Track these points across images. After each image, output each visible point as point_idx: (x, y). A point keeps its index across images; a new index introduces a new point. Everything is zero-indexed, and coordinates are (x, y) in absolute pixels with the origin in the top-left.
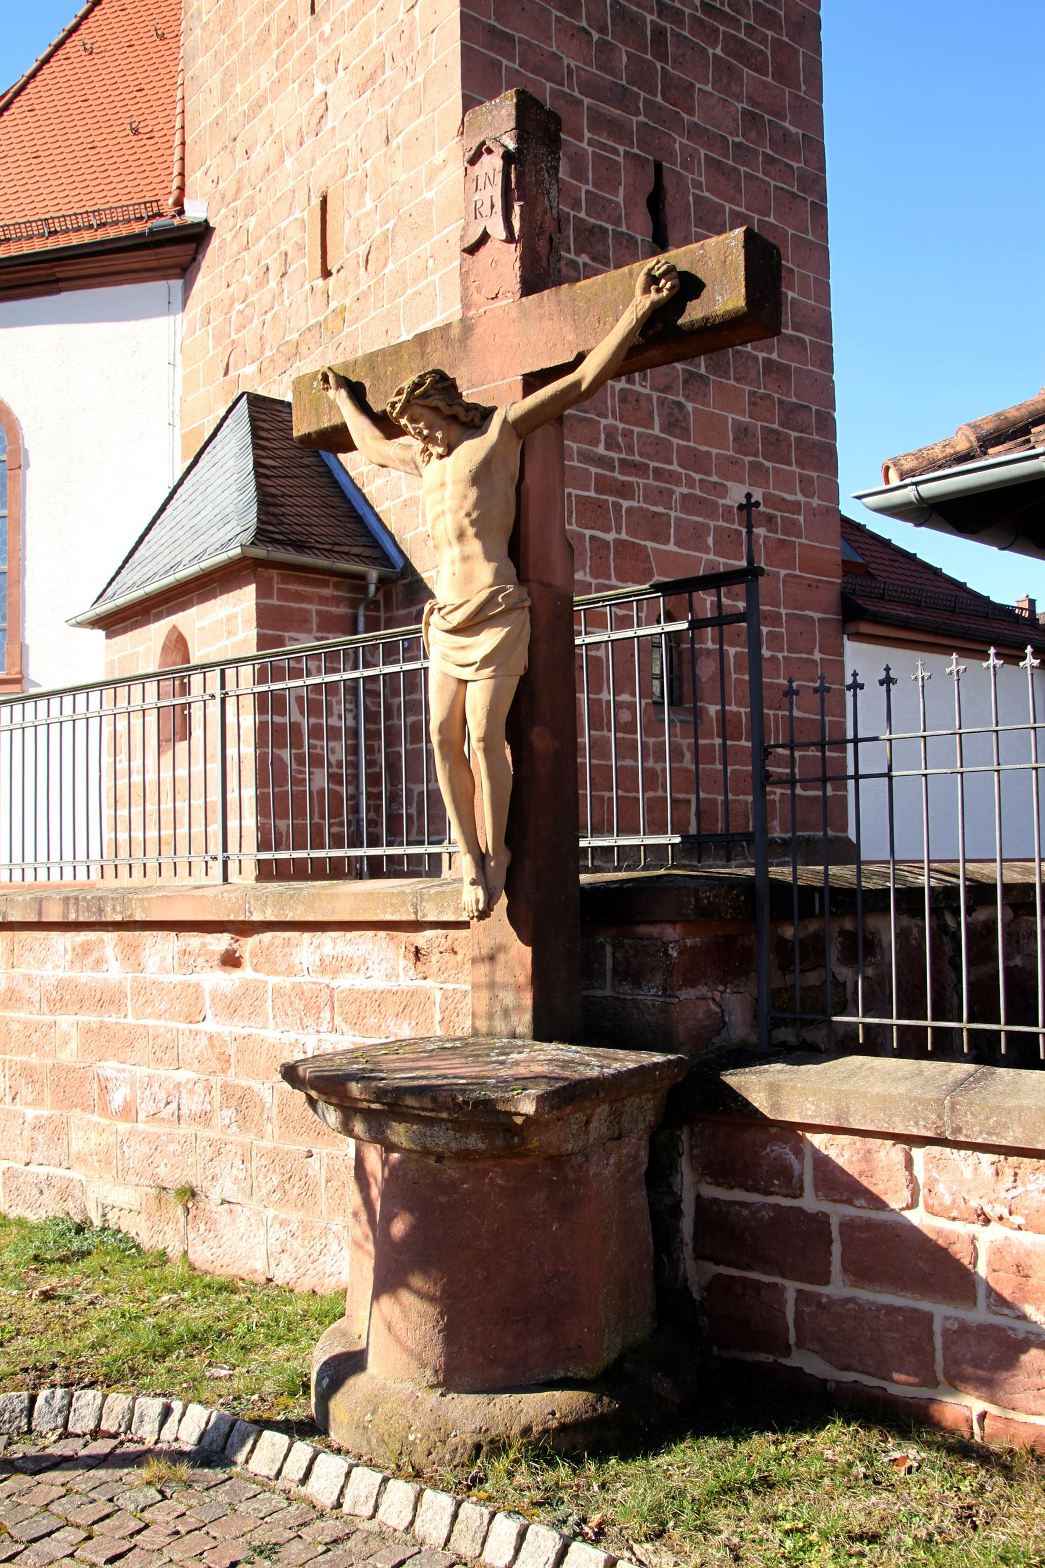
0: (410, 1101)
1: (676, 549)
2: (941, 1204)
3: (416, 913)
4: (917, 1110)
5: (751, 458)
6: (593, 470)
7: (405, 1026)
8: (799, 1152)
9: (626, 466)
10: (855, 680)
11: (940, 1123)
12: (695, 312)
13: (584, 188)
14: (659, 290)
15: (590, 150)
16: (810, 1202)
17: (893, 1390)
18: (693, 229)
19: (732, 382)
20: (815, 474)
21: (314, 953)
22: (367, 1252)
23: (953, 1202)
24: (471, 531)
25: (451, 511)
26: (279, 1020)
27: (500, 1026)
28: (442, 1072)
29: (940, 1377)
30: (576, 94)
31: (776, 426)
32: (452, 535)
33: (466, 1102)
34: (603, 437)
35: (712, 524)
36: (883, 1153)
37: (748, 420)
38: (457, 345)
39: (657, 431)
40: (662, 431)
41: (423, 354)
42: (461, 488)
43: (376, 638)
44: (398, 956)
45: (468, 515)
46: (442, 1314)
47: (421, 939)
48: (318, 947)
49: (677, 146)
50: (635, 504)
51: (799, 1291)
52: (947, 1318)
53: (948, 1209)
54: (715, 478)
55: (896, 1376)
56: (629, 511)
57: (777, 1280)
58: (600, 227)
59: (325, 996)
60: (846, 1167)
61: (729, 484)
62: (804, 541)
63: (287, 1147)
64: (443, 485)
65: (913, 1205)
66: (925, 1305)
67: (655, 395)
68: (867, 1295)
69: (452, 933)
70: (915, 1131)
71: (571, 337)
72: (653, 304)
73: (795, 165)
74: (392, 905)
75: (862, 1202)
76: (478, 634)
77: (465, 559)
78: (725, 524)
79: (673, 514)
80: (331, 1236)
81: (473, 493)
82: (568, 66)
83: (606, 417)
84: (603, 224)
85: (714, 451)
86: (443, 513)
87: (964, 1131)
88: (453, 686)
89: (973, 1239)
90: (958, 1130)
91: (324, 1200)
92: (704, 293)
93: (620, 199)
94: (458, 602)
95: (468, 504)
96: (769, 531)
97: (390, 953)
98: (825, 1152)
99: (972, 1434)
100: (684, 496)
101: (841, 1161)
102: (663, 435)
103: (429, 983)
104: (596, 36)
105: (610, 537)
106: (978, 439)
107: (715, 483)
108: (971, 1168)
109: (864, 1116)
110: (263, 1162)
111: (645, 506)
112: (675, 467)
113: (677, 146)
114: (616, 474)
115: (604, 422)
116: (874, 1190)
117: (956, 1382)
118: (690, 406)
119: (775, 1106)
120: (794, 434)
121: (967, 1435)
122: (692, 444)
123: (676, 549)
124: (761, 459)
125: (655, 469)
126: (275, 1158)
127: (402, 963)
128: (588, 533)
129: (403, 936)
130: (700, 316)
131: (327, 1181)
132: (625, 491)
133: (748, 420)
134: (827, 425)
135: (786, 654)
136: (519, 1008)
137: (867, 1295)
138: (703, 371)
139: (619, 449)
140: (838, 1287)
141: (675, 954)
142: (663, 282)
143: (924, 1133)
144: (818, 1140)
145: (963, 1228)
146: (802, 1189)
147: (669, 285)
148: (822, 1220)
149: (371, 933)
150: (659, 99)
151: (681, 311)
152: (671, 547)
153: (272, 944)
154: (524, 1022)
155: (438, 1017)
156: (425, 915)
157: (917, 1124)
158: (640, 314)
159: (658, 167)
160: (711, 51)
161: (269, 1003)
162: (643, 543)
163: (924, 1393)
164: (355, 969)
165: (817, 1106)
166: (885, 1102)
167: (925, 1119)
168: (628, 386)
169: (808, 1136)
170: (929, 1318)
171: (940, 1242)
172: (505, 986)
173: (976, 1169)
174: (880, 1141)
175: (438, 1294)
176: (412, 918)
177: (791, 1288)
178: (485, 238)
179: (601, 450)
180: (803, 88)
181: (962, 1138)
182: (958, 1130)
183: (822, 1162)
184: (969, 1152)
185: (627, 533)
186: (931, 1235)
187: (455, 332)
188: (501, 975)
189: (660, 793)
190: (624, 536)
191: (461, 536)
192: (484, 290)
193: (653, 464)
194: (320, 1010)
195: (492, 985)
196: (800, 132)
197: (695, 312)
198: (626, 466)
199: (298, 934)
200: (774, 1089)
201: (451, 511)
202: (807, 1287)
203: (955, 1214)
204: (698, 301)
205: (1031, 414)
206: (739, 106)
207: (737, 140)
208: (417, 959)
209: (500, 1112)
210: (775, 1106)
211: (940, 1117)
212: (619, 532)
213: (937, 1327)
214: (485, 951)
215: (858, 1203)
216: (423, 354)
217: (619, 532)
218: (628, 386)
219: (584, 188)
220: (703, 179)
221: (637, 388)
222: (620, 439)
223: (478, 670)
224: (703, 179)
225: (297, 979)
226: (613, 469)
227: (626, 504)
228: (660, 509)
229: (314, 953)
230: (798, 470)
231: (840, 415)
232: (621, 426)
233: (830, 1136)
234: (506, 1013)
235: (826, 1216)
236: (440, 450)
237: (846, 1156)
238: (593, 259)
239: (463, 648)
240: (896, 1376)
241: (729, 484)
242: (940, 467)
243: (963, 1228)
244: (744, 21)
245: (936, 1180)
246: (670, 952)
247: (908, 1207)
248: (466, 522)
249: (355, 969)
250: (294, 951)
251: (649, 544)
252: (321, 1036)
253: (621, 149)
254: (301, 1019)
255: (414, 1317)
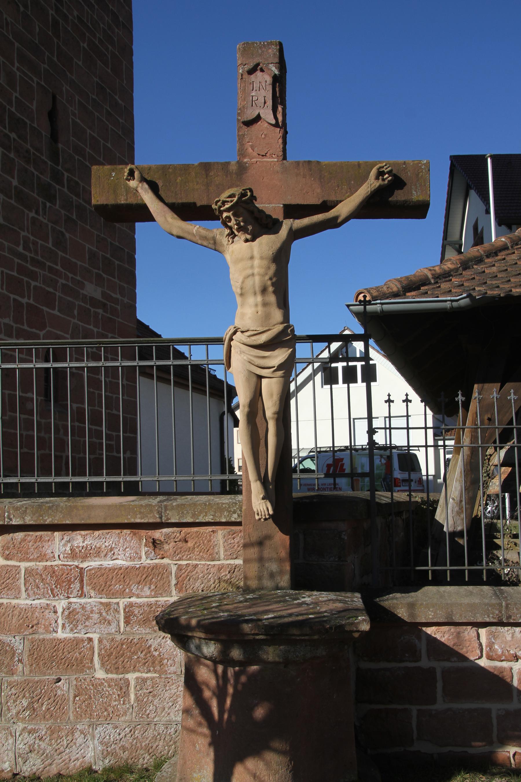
0: (295, 631)
1: (58, 314)
2: (496, 654)
3: (161, 518)
4: (489, 610)
5: (97, 271)
6: (16, 260)
7: (146, 589)
8: (419, 638)
9: (35, 262)
10: (407, 398)
11: (500, 615)
12: (399, 196)
13: (15, 94)
14: (383, 180)
15: (18, 73)
16: (425, 663)
17: (471, 751)
18: (71, 138)
19: (88, 227)
20: (125, 285)
21: (65, 545)
22: (205, 735)
23: (503, 652)
24: (271, 289)
25: (259, 274)
26: (31, 593)
27: (268, 583)
28: (279, 613)
29: (495, 739)
30: (11, 37)
31: (108, 256)
32: (258, 289)
33: (331, 628)
34: (22, 242)
35: (77, 303)
36: (466, 633)
37: (95, 249)
38: (234, 176)
39: (50, 245)
40: (53, 246)
41: (207, 175)
42: (265, 263)
43: (100, 343)
44: (140, 545)
45: (271, 279)
46: (290, 760)
47: (158, 534)
48: (69, 541)
49: (64, 89)
50: (38, 284)
51: (419, 710)
52: (499, 710)
53: (500, 656)
54: (78, 278)
55: (473, 744)
56: (35, 287)
57: (407, 706)
58: (23, 120)
59: (75, 573)
60: (446, 643)
61: (86, 283)
62: (120, 320)
63: (36, 679)
64: (252, 258)
65: (481, 657)
66: (487, 705)
67: (50, 225)
68: (455, 706)
69: (185, 530)
70: (488, 620)
71: (319, 191)
72: (380, 186)
73: (121, 120)
74: (140, 513)
75: (455, 659)
76: (274, 350)
77: (265, 304)
78: (83, 304)
79: (57, 294)
80: (77, 734)
81: (273, 267)
82: (6, 19)
83: (24, 231)
84: (24, 119)
85: (79, 263)
86: (253, 275)
87: (513, 618)
88: (254, 379)
89: (511, 669)
90: (509, 617)
91: (72, 709)
92: (405, 188)
93: (34, 107)
94: (261, 329)
95: (271, 272)
96: (105, 312)
97: (134, 542)
98: (435, 636)
99: (511, 764)
100: (63, 285)
101: (443, 640)
102: (53, 248)
103: (166, 561)
104: (22, 9)
105: (25, 301)
106: (402, 287)
107: (79, 281)
108: (510, 635)
109: (461, 616)
110: (13, 691)
111: (43, 286)
112: (59, 268)
113: (64, 89)
114: (28, 265)
115: (23, 233)
116: (461, 652)
117: (504, 741)
118: (67, 235)
119: (412, 615)
120: (117, 262)
121: (509, 765)
122: (68, 257)
123: (58, 314)
124: (101, 272)
125: (49, 266)
126: (26, 687)
127: (144, 550)
128: (12, 296)
129: (143, 533)
130: (403, 199)
131: (75, 696)
132: (33, 276)
133: (95, 249)
134: (132, 261)
135: (110, 379)
136: (281, 572)
137: (455, 706)
138: (74, 217)
139: (30, 251)
140: (441, 705)
141: (346, 538)
142: (387, 176)
143: (492, 620)
144: (430, 630)
145: (505, 664)
146: (421, 657)
147: (390, 178)
148: (432, 671)
149: (118, 531)
150: (55, 59)
151: (392, 194)
152: (56, 312)
153: (23, 540)
154: (285, 580)
155: (174, 582)
156: (168, 519)
157: (488, 616)
158: (373, 189)
159: (54, 98)
160: (82, 44)
161: (22, 581)
162: (41, 307)
163: (487, 749)
164: (102, 555)
165: (435, 613)
166: (472, 607)
167: (493, 613)
168: (36, 216)
169: (424, 629)
170: (489, 711)
171: (495, 673)
172: (270, 560)
173: (513, 635)
174: (465, 627)
175: (288, 748)
176: (158, 520)
177: (414, 709)
178: (258, 118)
179: (20, 249)
180: (125, 82)
181: (512, 621)
182: (509, 617)
183: (432, 641)
184: (510, 628)
185: (33, 300)
186: (492, 671)
187: (233, 167)
188: (267, 553)
189: (47, 451)
190: (31, 301)
191: (264, 291)
192: (256, 149)
193: (48, 264)
194: (70, 582)
195: (261, 560)
196: (123, 104)
197: (399, 196)
198: (35, 262)
199: (49, 533)
200: (411, 606)
201: (259, 274)
202: (424, 707)
203: (503, 658)
204: (402, 191)
205: (421, 280)
206: (95, 79)
207: (94, 97)
208: (155, 547)
209: (347, 631)
210: (412, 615)
211: (500, 612)
212: (29, 299)
213: (494, 715)
214: (254, 538)
215: (453, 660)
216: (207, 175)
217: (29, 299)
218: (36, 216)
219: (15, 94)
220: (77, 112)
221: (41, 218)
222: (31, 245)
223: (274, 371)
224: (77, 112)
225: (49, 563)
226: (27, 262)
227: (33, 283)
228: (51, 290)
229: (65, 545)
230: (118, 282)
231: (138, 257)
232: (32, 238)
233: (437, 627)
234: (272, 575)
235: (434, 669)
236: (249, 237)
237: (446, 637)
238: (19, 137)
239: (264, 357)
240: (473, 744)
241: (86, 283)
242: (387, 298)
243: (505, 664)
244: (98, 35)
245: (493, 643)
246: (343, 536)
247: (479, 658)
248: (269, 283)
249: (102, 555)
250: (46, 545)
251: (45, 308)
252: (72, 600)
253: (35, 79)
254: (52, 590)
255: (275, 766)
